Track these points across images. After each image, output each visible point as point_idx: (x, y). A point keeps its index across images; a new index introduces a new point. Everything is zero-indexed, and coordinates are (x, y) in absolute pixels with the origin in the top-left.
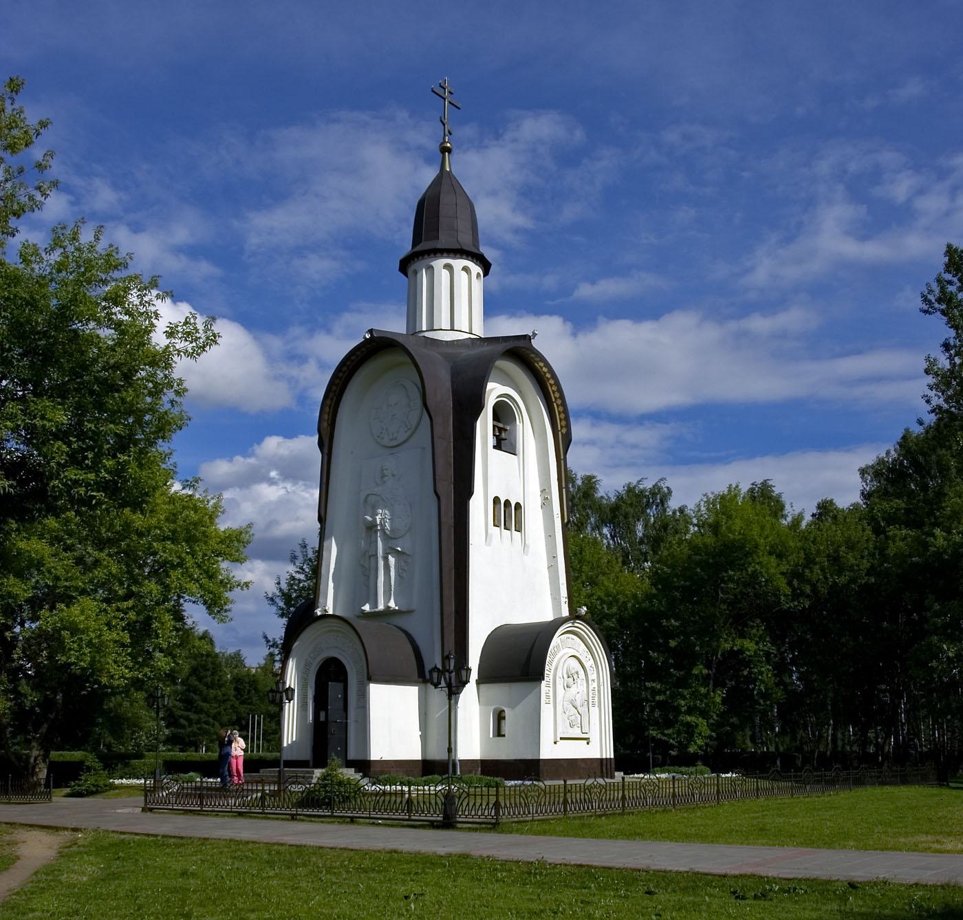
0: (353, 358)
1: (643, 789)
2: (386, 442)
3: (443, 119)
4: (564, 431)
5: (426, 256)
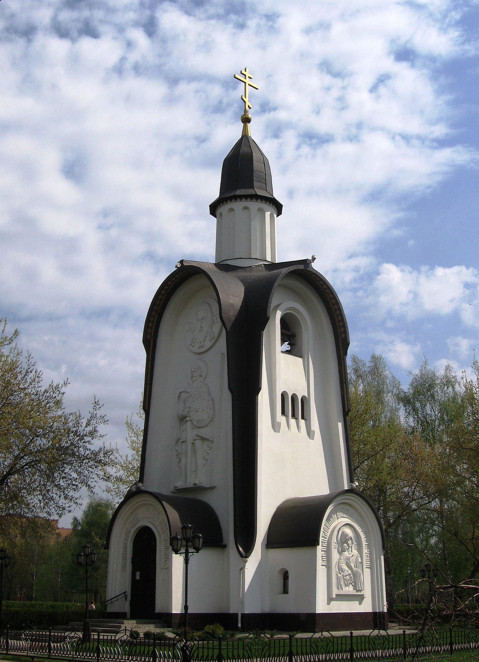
0: (173, 279)
1: (467, 636)
2: (196, 349)
3: (244, 98)
5: (229, 202)
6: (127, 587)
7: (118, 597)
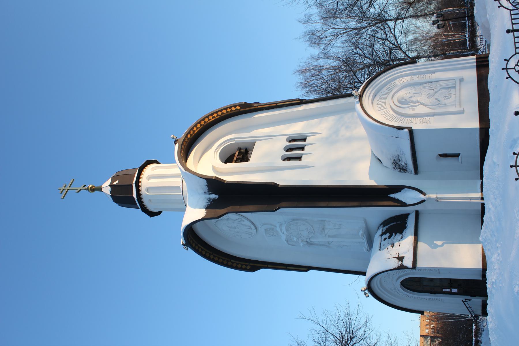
2: (253, 231)
6: (459, 299)
7: (468, 306)
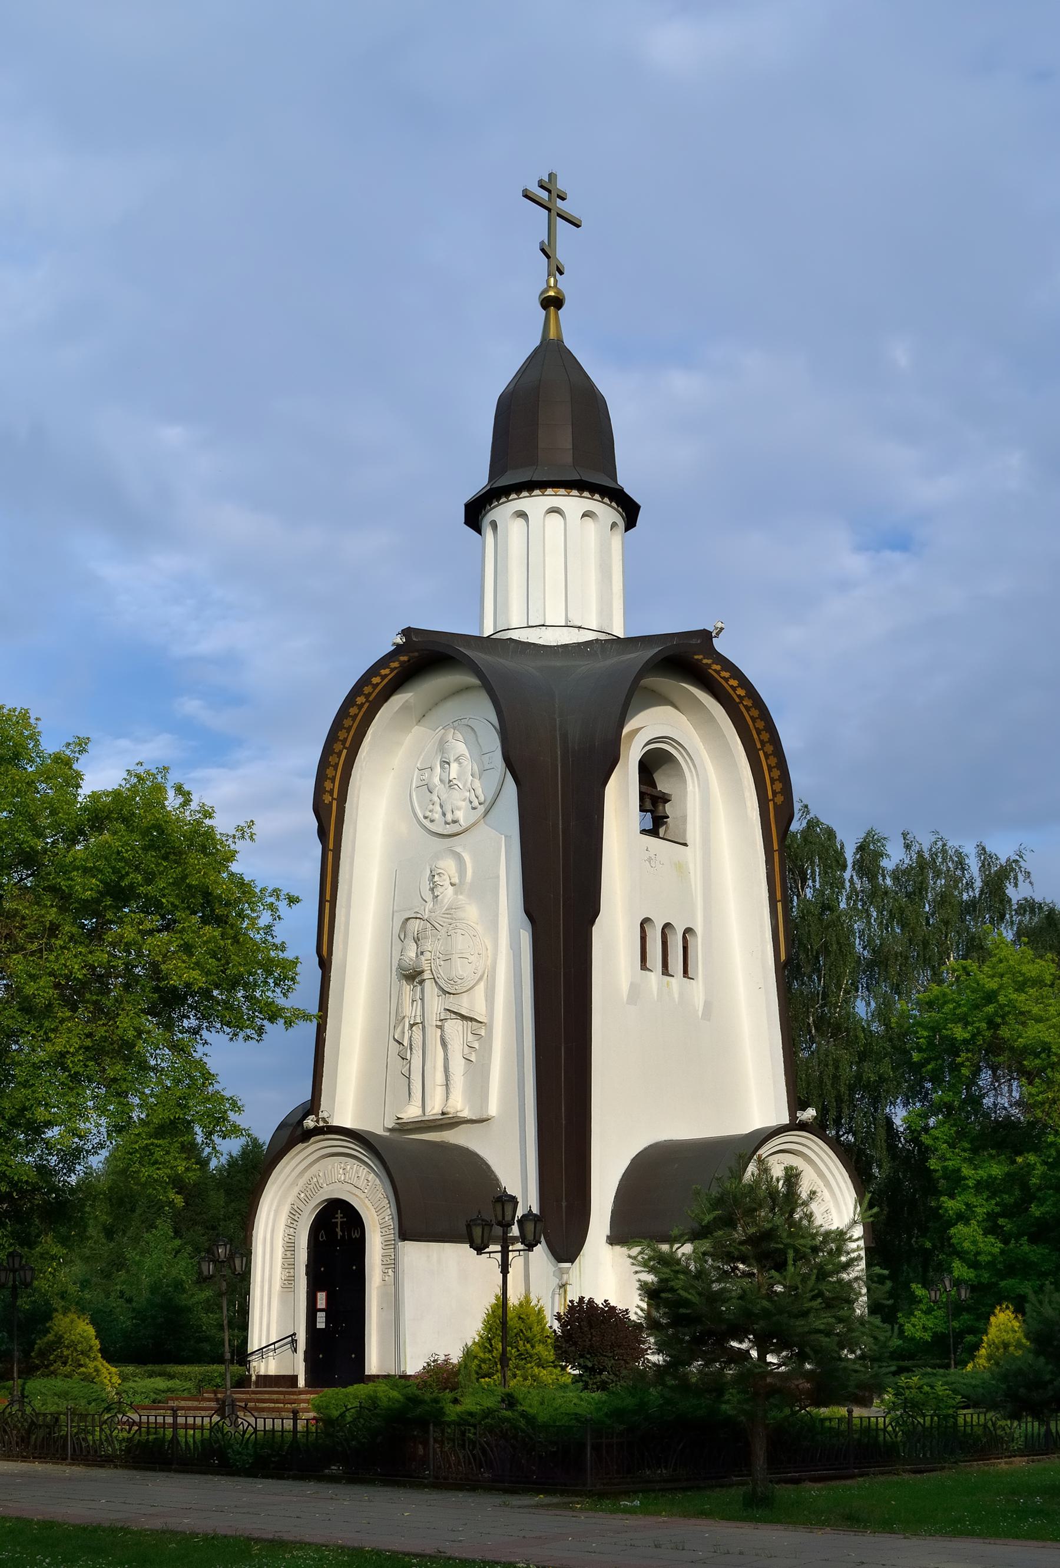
4: (779, 799)
